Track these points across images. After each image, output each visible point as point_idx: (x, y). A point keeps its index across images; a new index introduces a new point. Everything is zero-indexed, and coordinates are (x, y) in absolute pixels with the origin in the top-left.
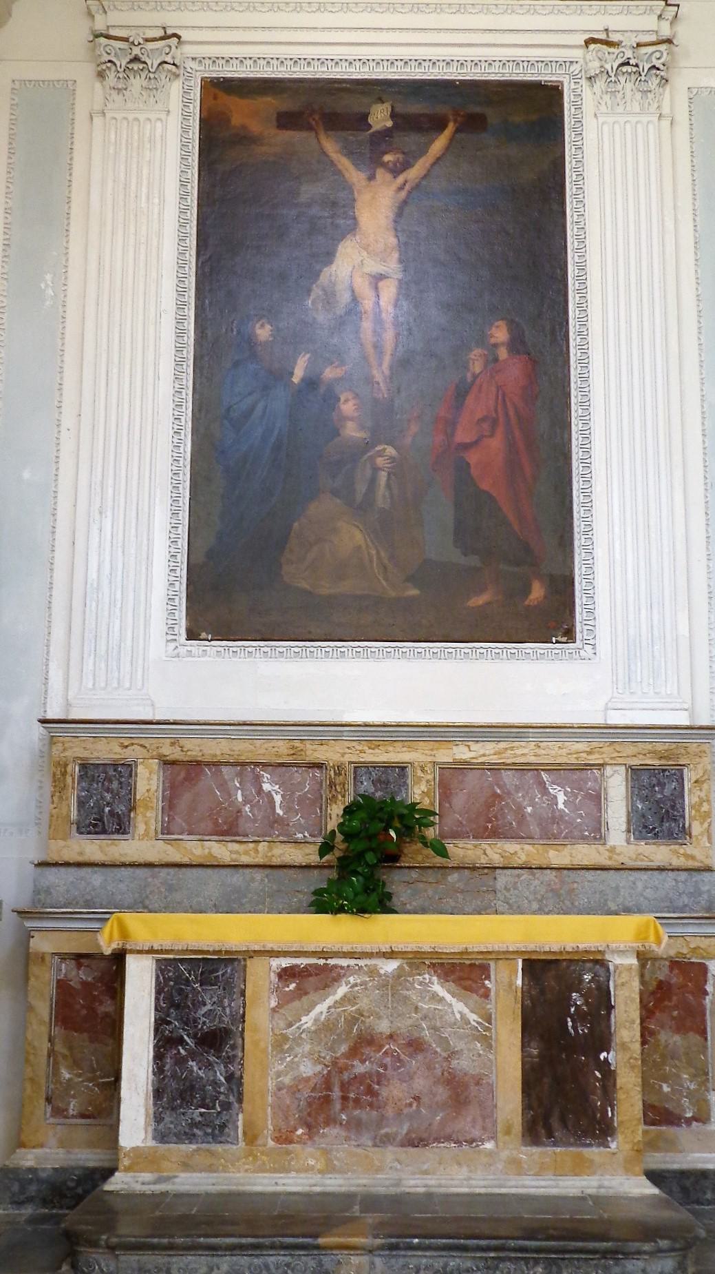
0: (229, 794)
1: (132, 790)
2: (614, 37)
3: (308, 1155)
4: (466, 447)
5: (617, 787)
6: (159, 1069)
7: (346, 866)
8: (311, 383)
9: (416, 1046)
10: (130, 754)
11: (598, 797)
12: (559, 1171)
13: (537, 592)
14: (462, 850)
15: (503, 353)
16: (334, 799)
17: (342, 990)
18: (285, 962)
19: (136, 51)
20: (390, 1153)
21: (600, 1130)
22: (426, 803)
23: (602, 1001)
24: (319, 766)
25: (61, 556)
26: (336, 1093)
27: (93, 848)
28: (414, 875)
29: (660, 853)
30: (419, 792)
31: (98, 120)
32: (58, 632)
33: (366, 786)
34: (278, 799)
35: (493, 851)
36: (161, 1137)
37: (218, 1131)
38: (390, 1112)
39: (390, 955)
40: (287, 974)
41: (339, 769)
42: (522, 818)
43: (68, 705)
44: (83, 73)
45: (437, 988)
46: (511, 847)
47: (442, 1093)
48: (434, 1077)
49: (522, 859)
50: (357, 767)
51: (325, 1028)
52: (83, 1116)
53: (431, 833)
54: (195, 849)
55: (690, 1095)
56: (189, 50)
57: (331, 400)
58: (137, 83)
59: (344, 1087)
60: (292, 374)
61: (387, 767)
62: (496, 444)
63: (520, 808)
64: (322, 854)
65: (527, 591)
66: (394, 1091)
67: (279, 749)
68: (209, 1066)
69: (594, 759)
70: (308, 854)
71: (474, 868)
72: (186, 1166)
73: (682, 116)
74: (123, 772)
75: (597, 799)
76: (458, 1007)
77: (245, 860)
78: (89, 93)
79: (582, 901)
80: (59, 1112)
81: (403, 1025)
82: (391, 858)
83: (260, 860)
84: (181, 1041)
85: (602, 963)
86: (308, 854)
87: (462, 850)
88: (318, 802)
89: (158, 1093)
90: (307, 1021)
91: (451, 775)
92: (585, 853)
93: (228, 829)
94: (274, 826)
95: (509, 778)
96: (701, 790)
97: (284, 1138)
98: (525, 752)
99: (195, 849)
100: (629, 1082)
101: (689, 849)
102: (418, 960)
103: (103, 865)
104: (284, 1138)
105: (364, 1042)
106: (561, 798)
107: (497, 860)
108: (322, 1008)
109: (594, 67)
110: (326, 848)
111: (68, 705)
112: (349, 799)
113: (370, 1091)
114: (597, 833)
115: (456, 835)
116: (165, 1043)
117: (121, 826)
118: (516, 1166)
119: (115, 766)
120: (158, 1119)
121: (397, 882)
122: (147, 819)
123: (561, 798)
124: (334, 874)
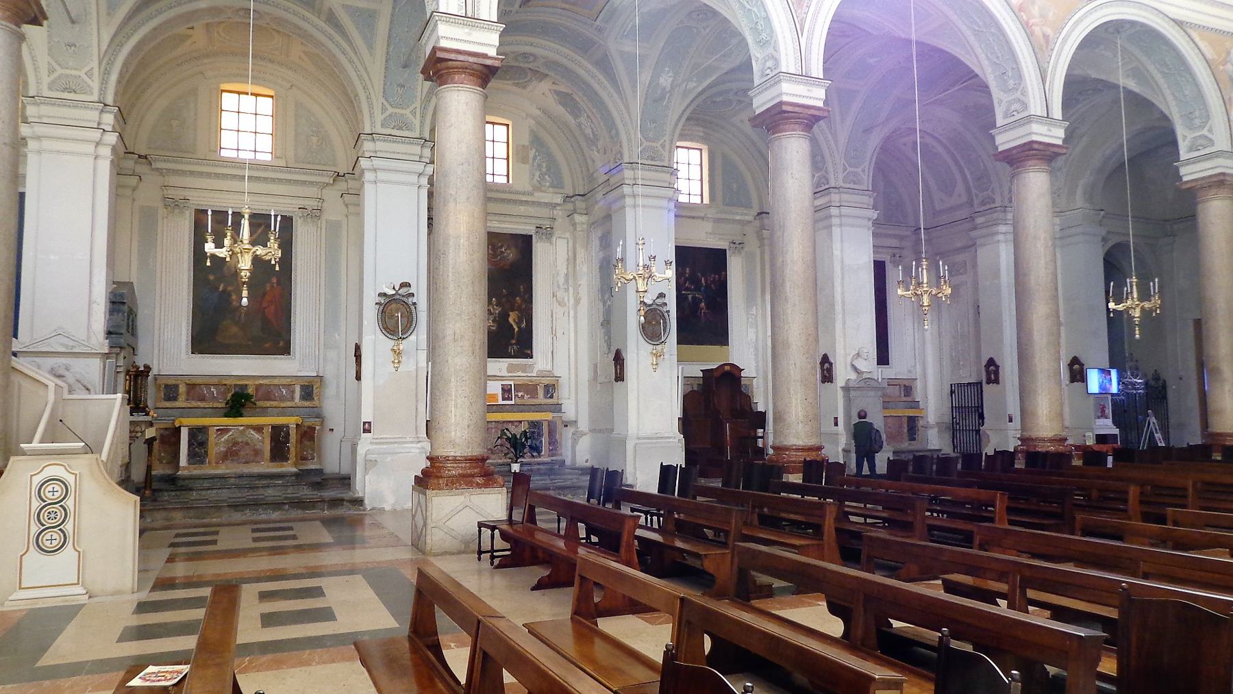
0: (203, 391)
1: (178, 391)
2: (307, 207)
3: (223, 467)
4: (265, 308)
5: (298, 390)
6: (189, 450)
7: (231, 407)
8: (224, 291)
9: (247, 444)
10: (177, 383)
11: (293, 391)
12: (277, 467)
13: (281, 344)
14: (260, 403)
15: (275, 285)
16: (229, 393)
17: (231, 433)
18: (218, 428)
19: (177, 203)
20: (241, 465)
21: (287, 459)
22: (251, 393)
23: (288, 434)
24: (226, 385)
25: (156, 332)
26: (229, 454)
27: (168, 404)
28: (248, 409)
29: (307, 404)
30: (250, 391)
31: (165, 220)
32: (156, 351)
33: (237, 389)
34: (215, 392)
35: (268, 404)
36: (189, 464)
37: (202, 462)
38: (241, 457)
39: (241, 426)
40: (218, 430)
41: (231, 385)
42: (275, 397)
43: (159, 370)
44: (160, 204)
45: (252, 432)
46: (272, 403)
47: (252, 453)
48: (22, 38)
49: (274, 405)
50: (235, 385)
51: (227, 440)
52: (168, 463)
53: (253, 400)
54: (194, 404)
55: (311, 454)
56: (191, 202)
57: (230, 295)
58: (176, 211)
59: (231, 453)
60: (219, 289)
61: (242, 385)
62: (273, 308)
63: (275, 394)
64: (226, 405)
65: (279, 343)
66: (242, 453)
67: (215, 381)
68: (200, 449)
69: (293, 383)
70: (223, 405)
71: (262, 408)
72: (195, 469)
73: (324, 227)
74: (177, 386)
75: (293, 392)
76: (257, 436)
77: (207, 406)
78: (162, 211)
79: (287, 414)
80: (161, 463)
81: (245, 440)
82: (243, 406)
83: (211, 406)
84: (193, 444)
85: (288, 427)
86: (223, 405)
87: (260, 403)
88: (224, 393)
89: (188, 455)
90: (223, 440)
91: (258, 387)
92: (289, 404)
93: (203, 399)
94: (214, 398)
95: (272, 387)
96: (797, 345)
97: (217, 463)
98: (276, 382)
99: (194, 404)
100: (293, 450)
101: (314, 403)
102: (248, 427)
103: (171, 408)
104: (217, 463)
105: (235, 443)
106: (284, 392)
107: (268, 405)
108: (226, 437)
109: (301, 215)
110: (226, 404)
111: (159, 370)
112: (233, 392)
113: (236, 453)
114: (293, 399)
115: (259, 400)
116: (190, 444)
117: (175, 399)
118: (268, 467)
119: (174, 385)
120: (189, 460)
121: (244, 411)
122: (182, 398)
123: (284, 392)
124: (229, 409)
